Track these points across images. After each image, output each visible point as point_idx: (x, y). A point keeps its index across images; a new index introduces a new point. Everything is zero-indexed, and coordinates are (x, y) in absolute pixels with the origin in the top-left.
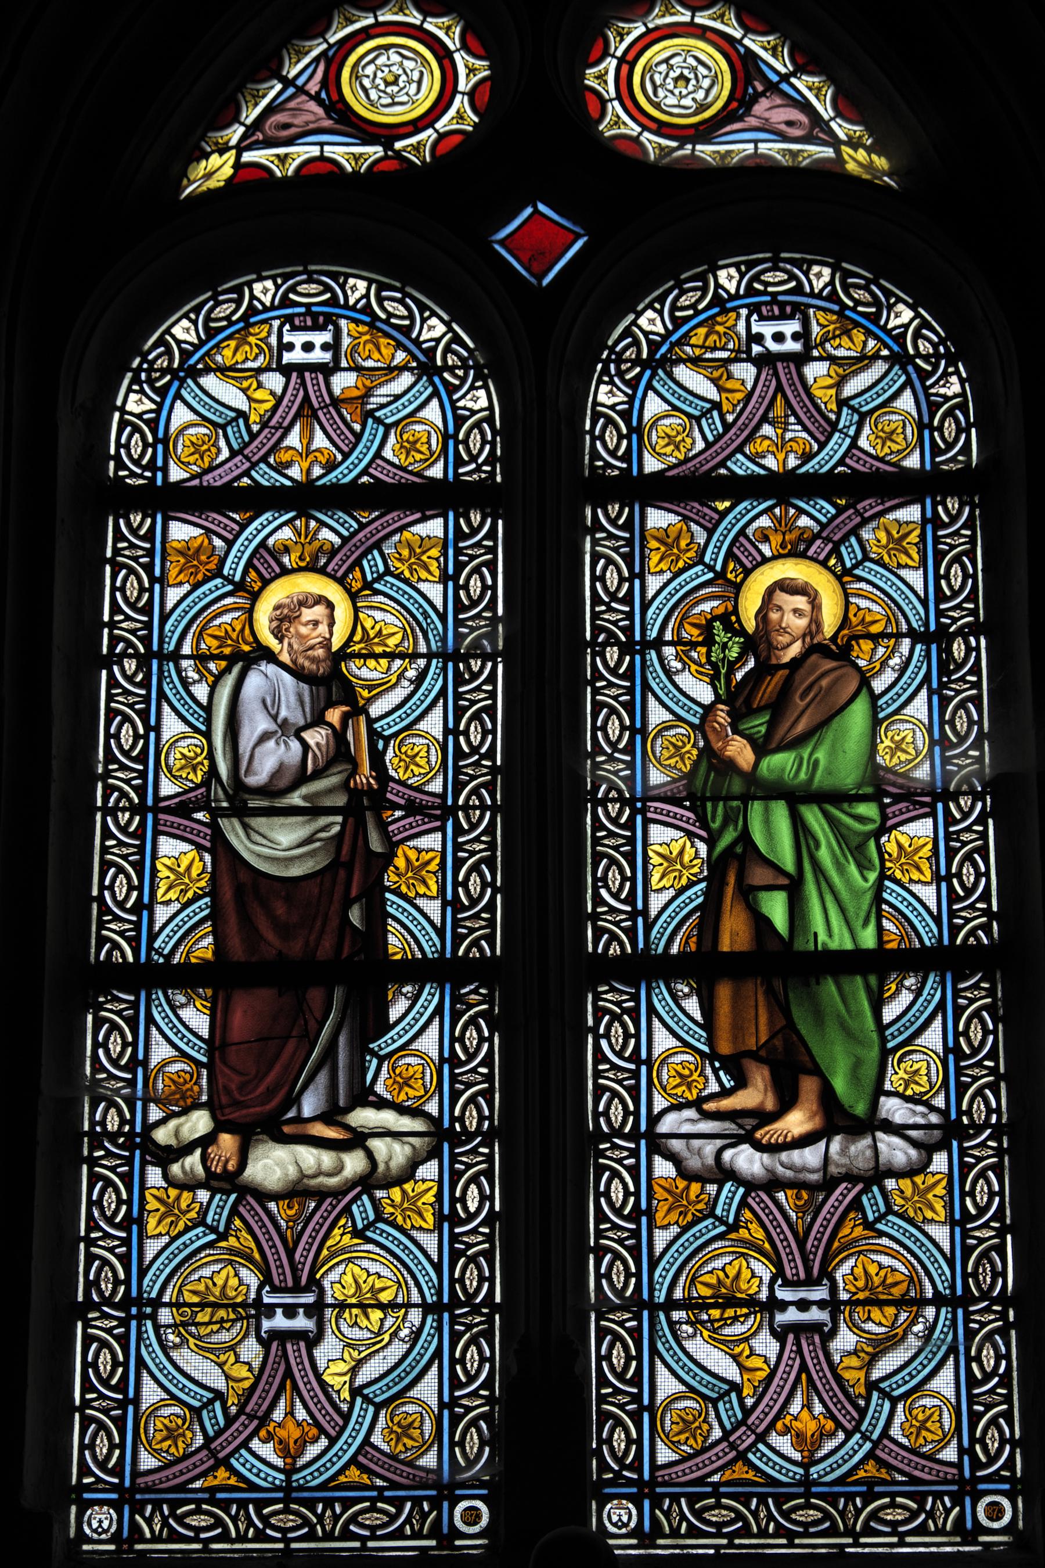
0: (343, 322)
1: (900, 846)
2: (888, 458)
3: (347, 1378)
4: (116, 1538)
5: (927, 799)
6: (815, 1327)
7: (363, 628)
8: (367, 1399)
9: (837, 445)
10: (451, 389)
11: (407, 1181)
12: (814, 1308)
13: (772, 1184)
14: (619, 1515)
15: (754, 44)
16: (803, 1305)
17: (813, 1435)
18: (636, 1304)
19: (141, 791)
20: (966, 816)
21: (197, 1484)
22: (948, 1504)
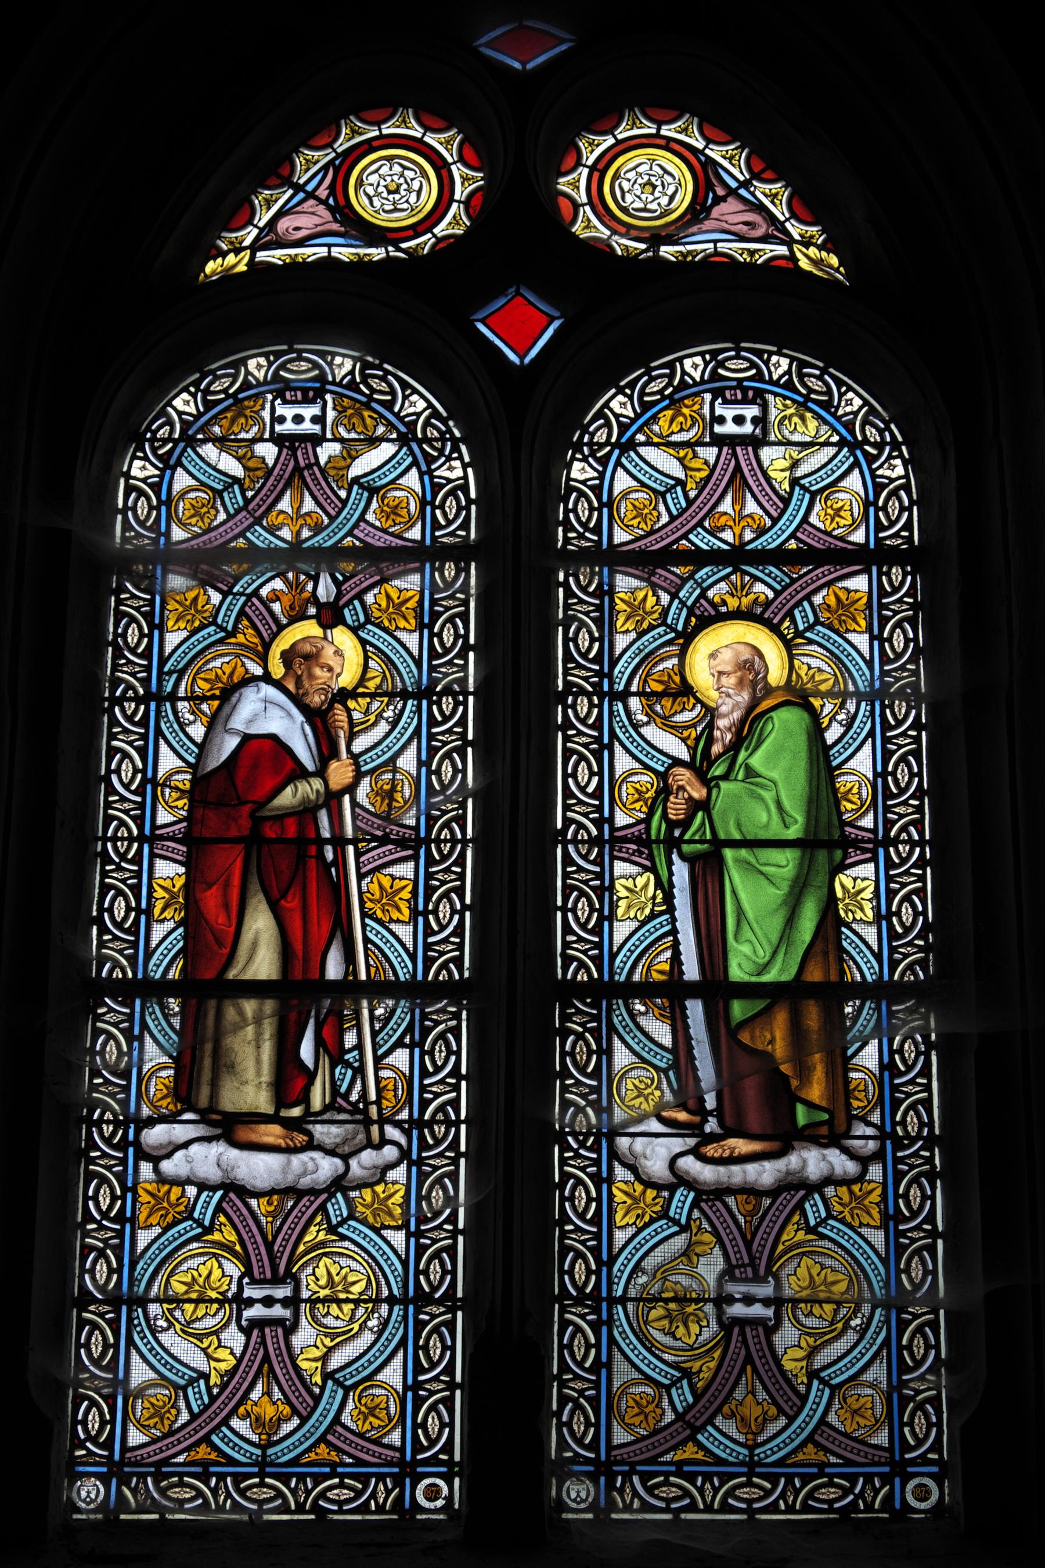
0: (770, 398)
1: (381, 887)
2: (835, 533)
3: (804, 1363)
4: (592, 1508)
5: (871, 846)
6: (279, 1322)
7: (798, 675)
8: (337, 1382)
9: (789, 522)
10: (870, 459)
11: (378, 1183)
12: (278, 1306)
13: (720, 1192)
14: (577, 1492)
15: (715, 153)
16: (268, 1302)
17: (756, 1419)
18: (422, 1299)
19: (139, 821)
20: (904, 861)
21: (668, 1457)
22: (390, 1486)
